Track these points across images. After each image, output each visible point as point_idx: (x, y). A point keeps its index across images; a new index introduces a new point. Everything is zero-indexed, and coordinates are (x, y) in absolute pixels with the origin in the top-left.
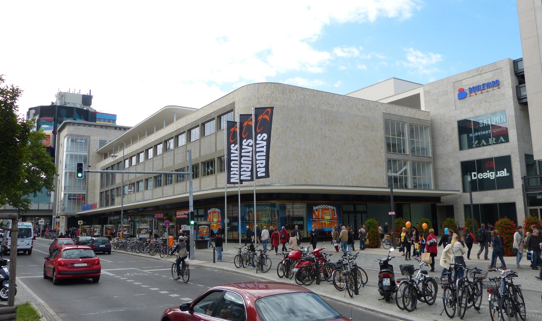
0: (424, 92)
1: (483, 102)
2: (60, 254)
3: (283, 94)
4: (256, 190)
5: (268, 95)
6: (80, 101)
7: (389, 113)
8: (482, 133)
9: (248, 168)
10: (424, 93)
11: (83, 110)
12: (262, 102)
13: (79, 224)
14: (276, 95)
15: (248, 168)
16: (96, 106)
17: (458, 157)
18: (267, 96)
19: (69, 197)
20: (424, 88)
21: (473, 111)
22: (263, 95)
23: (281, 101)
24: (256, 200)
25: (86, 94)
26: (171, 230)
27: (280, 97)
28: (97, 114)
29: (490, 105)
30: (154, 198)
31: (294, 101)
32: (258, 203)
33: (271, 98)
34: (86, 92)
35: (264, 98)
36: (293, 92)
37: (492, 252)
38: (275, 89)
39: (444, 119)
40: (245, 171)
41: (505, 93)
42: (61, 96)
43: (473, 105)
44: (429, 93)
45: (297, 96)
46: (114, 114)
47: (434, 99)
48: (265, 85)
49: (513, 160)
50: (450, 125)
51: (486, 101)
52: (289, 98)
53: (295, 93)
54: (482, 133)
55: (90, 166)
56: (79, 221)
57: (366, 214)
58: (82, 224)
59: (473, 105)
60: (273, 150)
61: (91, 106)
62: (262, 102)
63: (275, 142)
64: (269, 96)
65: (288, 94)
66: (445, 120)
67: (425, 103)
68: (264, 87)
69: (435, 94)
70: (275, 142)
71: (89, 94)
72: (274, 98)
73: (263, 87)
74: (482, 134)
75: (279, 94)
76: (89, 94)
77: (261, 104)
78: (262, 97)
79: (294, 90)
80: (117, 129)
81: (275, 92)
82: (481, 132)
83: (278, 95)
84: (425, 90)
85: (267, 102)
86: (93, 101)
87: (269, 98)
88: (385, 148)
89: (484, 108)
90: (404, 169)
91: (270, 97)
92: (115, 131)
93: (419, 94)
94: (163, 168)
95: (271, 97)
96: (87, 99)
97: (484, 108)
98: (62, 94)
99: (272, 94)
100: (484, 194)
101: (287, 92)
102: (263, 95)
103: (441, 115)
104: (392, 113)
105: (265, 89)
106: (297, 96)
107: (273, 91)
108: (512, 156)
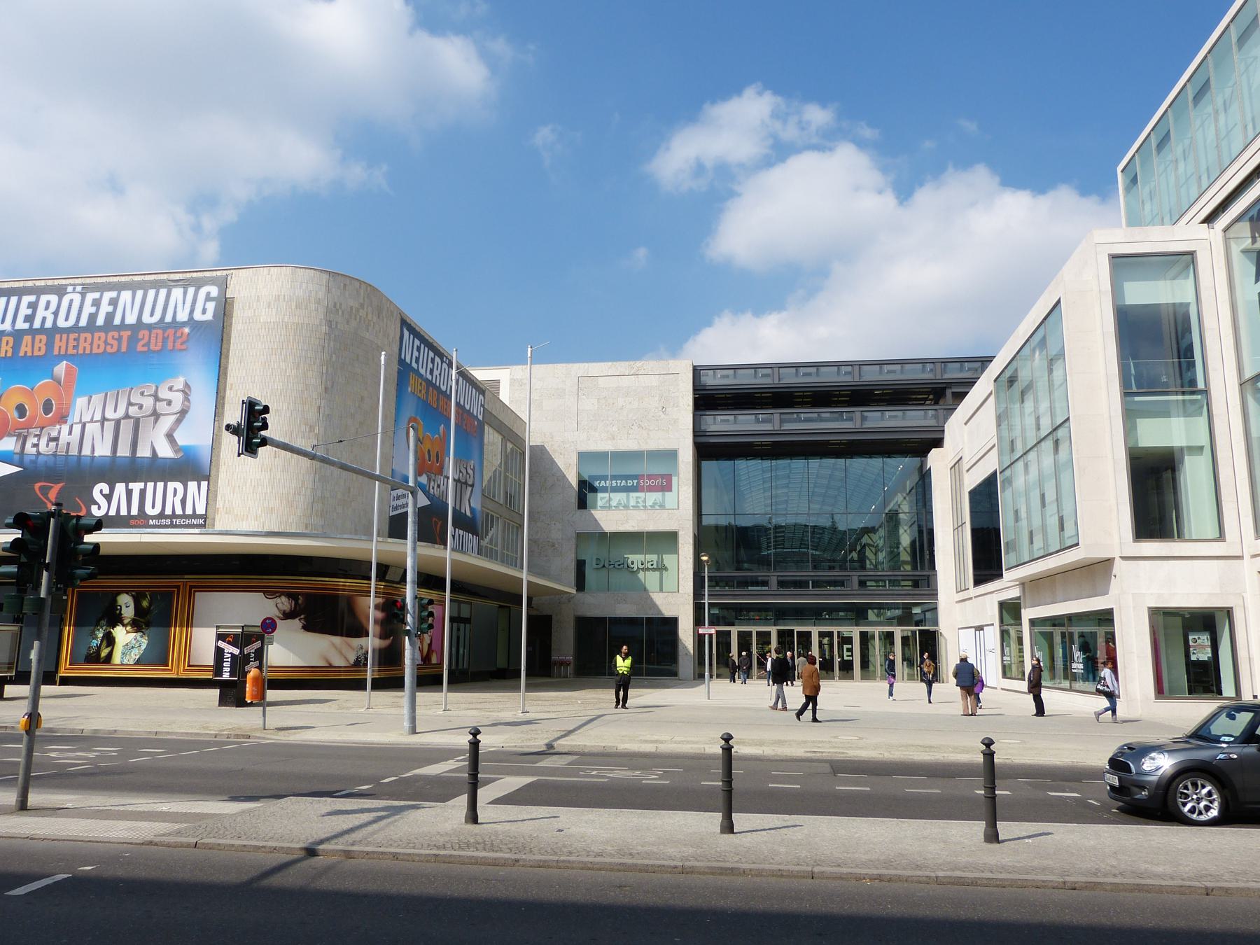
0: (511, 379)
1: (635, 427)
5: (351, 308)
8: (621, 483)
9: (175, 490)
15: (175, 490)
17: (573, 522)
18: (349, 310)
20: (511, 371)
21: (614, 439)
22: (341, 304)
29: (648, 434)
32: (369, 582)
33: (358, 317)
38: (366, 299)
39: (550, 443)
40: (183, 502)
41: (678, 419)
43: (615, 429)
44: (521, 386)
49: (680, 541)
50: (562, 456)
51: (640, 426)
54: (621, 483)
59: (615, 429)
62: (337, 322)
64: (354, 311)
65: (385, 320)
66: (552, 445)
68: (345, 285)
74: (619, 485)
77: (333, 326)
81: (365, 306)
82: (619, 482)
83: (370, 317)
84: (515, 378)
87: (353, 317)
88: (1182, 527)
89: (635, 439)
91: (364, 321)
93: (498, 381)
95: (358, 317)
97: (635, 439)
99: (361, 311)
100: (619, 599)
102: (341, 304)
103: (545, 435)
105: (347, 293)
107: (361, 301)
108: (681, 534)
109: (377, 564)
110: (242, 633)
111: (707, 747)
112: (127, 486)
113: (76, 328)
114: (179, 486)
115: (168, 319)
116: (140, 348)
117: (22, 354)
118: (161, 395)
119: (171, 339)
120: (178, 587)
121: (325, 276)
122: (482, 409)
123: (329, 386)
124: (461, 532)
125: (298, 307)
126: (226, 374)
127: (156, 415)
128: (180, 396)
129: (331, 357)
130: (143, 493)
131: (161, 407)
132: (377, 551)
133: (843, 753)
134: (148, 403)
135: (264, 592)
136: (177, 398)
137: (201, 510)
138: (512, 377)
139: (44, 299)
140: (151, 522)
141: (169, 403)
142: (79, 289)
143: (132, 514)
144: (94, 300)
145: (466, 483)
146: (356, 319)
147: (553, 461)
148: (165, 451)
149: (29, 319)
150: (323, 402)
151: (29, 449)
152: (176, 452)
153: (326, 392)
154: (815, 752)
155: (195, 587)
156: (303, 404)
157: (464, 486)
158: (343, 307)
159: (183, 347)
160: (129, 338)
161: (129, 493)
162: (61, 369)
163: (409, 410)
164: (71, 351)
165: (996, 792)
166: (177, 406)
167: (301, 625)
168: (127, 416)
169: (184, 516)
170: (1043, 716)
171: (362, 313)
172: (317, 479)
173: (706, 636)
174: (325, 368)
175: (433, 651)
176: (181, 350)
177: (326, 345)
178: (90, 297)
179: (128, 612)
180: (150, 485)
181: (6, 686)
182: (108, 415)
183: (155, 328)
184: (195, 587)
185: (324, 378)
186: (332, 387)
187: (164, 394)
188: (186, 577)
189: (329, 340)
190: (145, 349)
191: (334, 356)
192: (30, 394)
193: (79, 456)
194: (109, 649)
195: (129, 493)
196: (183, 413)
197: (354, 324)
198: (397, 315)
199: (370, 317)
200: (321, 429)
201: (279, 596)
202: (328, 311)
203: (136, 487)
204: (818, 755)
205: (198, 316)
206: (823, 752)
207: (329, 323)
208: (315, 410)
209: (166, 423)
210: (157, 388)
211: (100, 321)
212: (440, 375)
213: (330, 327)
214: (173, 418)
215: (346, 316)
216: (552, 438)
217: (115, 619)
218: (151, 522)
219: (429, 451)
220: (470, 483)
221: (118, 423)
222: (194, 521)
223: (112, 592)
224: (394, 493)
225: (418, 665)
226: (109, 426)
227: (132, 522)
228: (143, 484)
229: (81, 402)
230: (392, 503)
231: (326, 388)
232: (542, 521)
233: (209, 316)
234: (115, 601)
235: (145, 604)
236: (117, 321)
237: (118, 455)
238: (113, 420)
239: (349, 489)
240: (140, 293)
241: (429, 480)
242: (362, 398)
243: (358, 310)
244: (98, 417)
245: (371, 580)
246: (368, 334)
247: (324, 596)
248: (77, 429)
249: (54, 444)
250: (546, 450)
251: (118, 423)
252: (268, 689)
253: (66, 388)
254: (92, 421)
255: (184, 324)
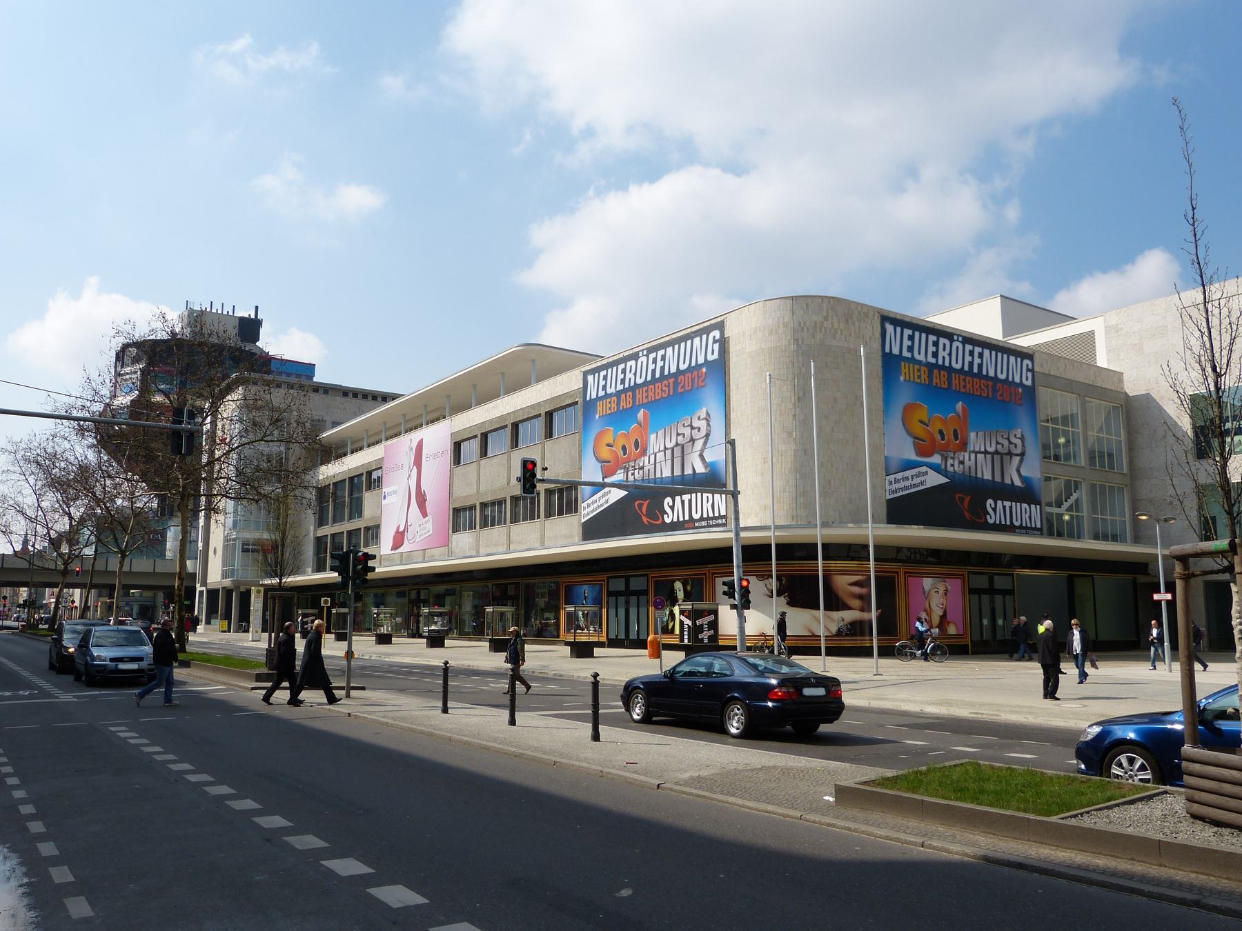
0: (1106, 327)
2: (941, 654)
3: (847, 321)
4: (775, 537)
6: (233, 331)
7: (1047, 372)
10: (1105, 330)
11: (240, 350)
12: (803, 339)
13: (322, 604)
14: (832, 324)
16: (272, 343)
19: (243, 545)
20: (1105, 319)
22: (805, 322)
23: (844, 339)
24: (777, 560)
25: (246, 315)
26: (74, 632)
27: (841, 330)
28: (272, 361)
30: (482, 551)
31: (868, 340)
32: (816, 562)
33: (823, 331)
34: (245, 312)
35: (808, 329)
36: (866, 319)
37: (1042, 685)
38: (830, 311)
42: (197, 318)
45: (873, 328)
46: (309, 362)
47: (1132, 344)
48: (810, 302)
52: (858, 332)
53: (869, 320)
55: (546, 469)
56: (323, 599)
57: (1012, 596)
58: (329, 605)
60: (829, 449)
61: (257, 344)
62: (803, 339)
63: (833, 430)
64: (818, 326)
65: (857, 324)
67: (1107, 353)
68: (807, 305)
69: (1134, 333)
70: (833, 430)
71: (253, 316)
72: (828, 331)
73: (805, 305)
75: (839, 322)
76: (253, 316)
77: (800, 343)
78: (803, 328)
79: (866, 315)
80: (347, 396)
81: (830, 318)
85: (813, 340)
86: (264, 332)
87: (818, 330)
90: (1075, 496)
91: (820, 329)
92: (344, 399)
93: (1093, 332)
94: (508, 484)
95: (823, 330)
96: (250, 327)
98: (195, 315)
99: (826, 322)
101: (855, 318)
102: (805, 322)
104: (1052, 374)
105: (810, 310)
106: (873, 328)
107: (825, 314)
109: (874, 546)
110: (692, 608)
111: (902, 704)
112: (681, 498)
113: (646, 383)
114: (710, 496)
115: (693, 364)
116: (680, 390)
117: (621, 409)
118: (694, 425)
119: (696, 379)
120: (705, 574)
121: (789, 302)
122: (1030, 374)
123: (801, 395)
124: (1007, 504)
125: (770, 333)
126: (729, 400)
127: (693, 440)
128: (704, 422)
129: (801, 369)
130: (690, 501)
131: (695, 433)
132: (821, 535)
133: (998, 715)
134: (687, 431)
135: (756, 575)
136: (703, 424)
137: (723, 513)
138: (1106, 324)
139: (629, 364)
140: (697, 524)
141: (699, 429)
142: (645, 352)
143: (721, 514)
144: (654, 359)
145: (1010, 454)
146: (821, 331)
147: (1161, 409)
148: (700, 469)
149: (623, 381)
150: (797, 410)
151: (631, 478)
152: (706, 467)
153: (799, 401)
154: (977, 713)
155: (716, 573)
156: (781, 415)
157: (1007, 458)
158: (807, 325)
159: (703, 384)
160: (673, 383)
161: (683, 502)
162: (641, 415)
163: (904, 397)
164: (645, 401)
165: (449, 683)
166: (703, 432)
167: (786, 601)
168: (677, 445)
169: (714, 518)
170: (391, 643)
171: (827, 324)
172: (798, 477)
173: (1163, 602)
174: (796, 380)
175: (948, 623)
176: (702, 386)
177: (796, 361)
178: (652, 356)
179: (680, 595)
180: (694, 495)
181: (595, 649)
182: (667, 446)
183: (687, 372)
184: (716, 573)
185: (796, 389)
186: (804, 395)
187: (696, 423)
188: (709, 566)
189: (798, 356)
190: (683, 390)
191: (803, 369)
192: (626, 436)
193: (655, 478)
194: (673, 623)
195: (683, 502)
196: (707, 435)
197: (819, 336)
198: (874, 315)
199: (836, 325)
200: (798, 434)
201: (767, 578)
202: (794, 331)
203: (686, 497)
204: (980, 716)
205: (710, 358)
206: (983, 714)
207: (796, 341)
208: (791, 418)
209: (699, 445)
210: (691, 419)
211: (658, 375)
212: (950, 355)
213: (797, 344)
214: (702, 440)
215: (810, 331)
216: (1157, 383)
217: (674, 601)
218: (697, 524)
219: (941, 432)
220: (1019, 451)
221: (673, 449)
222: (720, 521)
223: (667, 581)
224: (892, 478)
225: (826, 636)
226: (669, 452)
227: (686, 526)
228: (689, 495)
229: (653, 437)
230: (888, 487)
231: (799, 398)
232: (1156, 478)
233: (716, 356)
234: (673, 587)
235: (689, 588)
236: (666, 373)
237: (675, 475)
238: (670, 448)
239: (830, 481)
240: (676, 347)
241: (945, 459)
242: (835, 400)
243: (823, 322)
244: (662, 448)
245: (869, 561)
246: (835, 341)
247: (801, 576)
248: (652, 457)
249: (641, 472)
250: (1153, 398)
251: (673, 449)
252: (663, 650)
253: (644, 429)
254: (659, 451)
255: (702, 365)
